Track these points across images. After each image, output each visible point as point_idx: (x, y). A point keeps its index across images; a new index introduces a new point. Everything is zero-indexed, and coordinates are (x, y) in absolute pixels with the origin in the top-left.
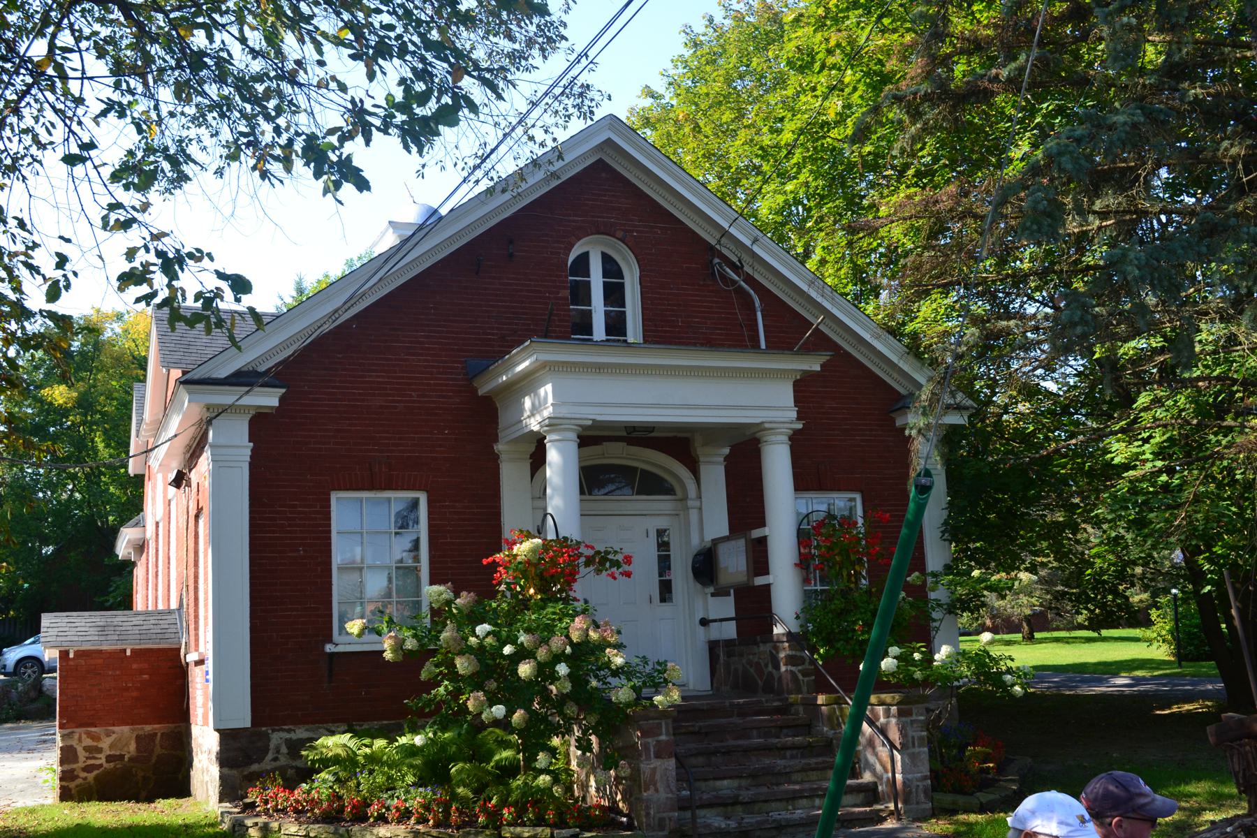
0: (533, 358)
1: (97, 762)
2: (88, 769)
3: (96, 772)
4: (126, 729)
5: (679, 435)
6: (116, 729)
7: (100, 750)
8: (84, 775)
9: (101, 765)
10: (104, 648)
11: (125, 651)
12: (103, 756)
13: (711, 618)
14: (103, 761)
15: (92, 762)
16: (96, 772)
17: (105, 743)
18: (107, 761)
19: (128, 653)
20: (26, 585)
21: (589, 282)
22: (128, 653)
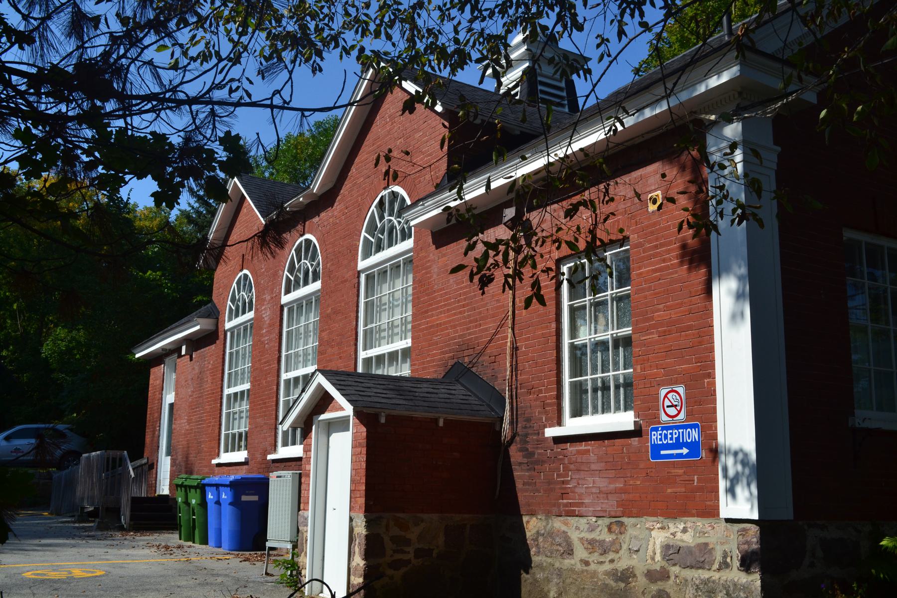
0: (697, 93)
1: (406, 557)
2: (395, 565)
3: (403, 570)
4: (435, 516)
5: (177, 324)
6: (425, 516)
7: (408, 542)
8: (390, 572)
9: (409, 561)
10: (417, 415)
11: (436, 421)
12: (411, 549)
13: (20, 16)
14: (411, 556)
15: (398, 556)
16: (403, 570)
17: (413, 534)
18: (416, 557)
19: (441, 424)
20: (78, 356)
21: (389, 353)
22: (441, 424)
